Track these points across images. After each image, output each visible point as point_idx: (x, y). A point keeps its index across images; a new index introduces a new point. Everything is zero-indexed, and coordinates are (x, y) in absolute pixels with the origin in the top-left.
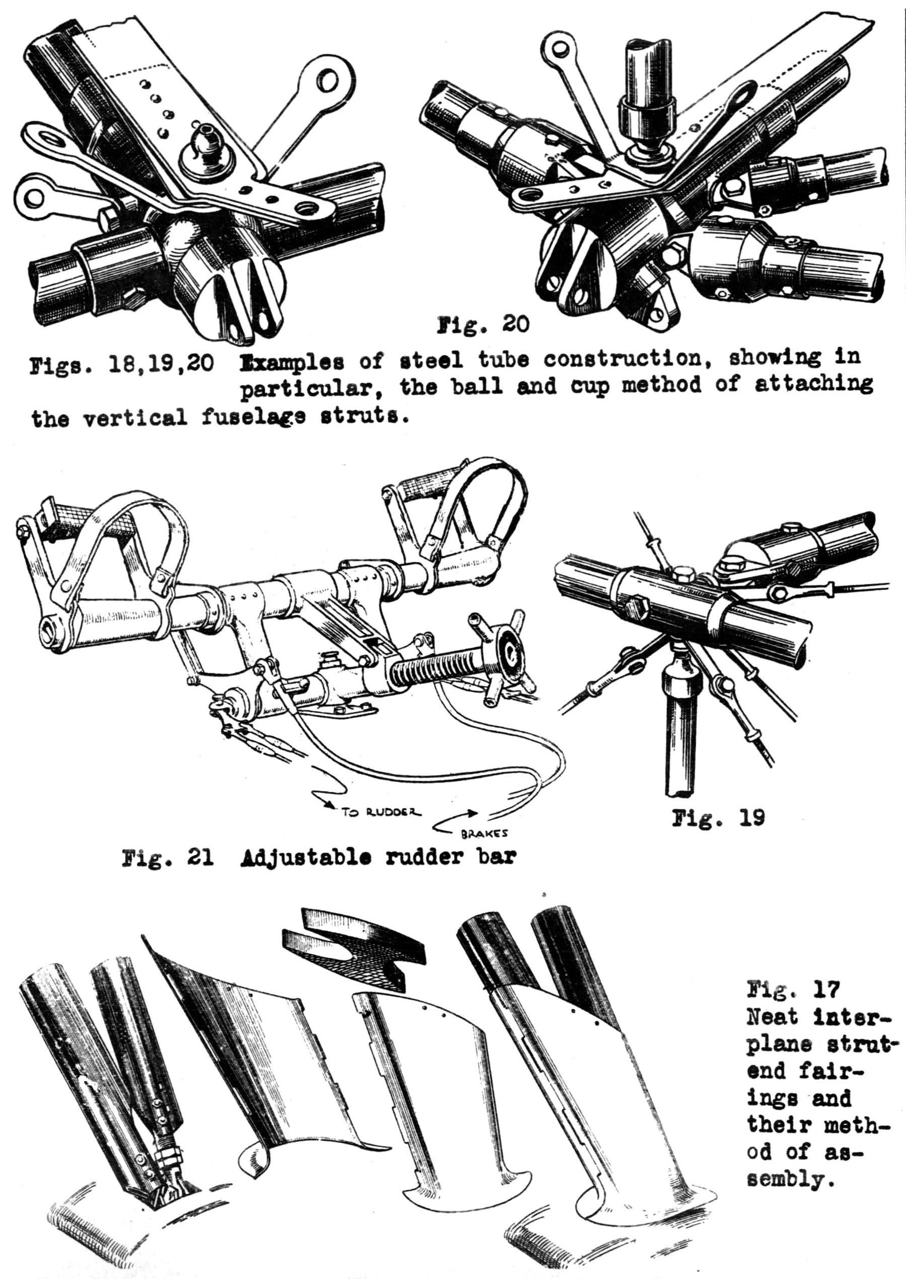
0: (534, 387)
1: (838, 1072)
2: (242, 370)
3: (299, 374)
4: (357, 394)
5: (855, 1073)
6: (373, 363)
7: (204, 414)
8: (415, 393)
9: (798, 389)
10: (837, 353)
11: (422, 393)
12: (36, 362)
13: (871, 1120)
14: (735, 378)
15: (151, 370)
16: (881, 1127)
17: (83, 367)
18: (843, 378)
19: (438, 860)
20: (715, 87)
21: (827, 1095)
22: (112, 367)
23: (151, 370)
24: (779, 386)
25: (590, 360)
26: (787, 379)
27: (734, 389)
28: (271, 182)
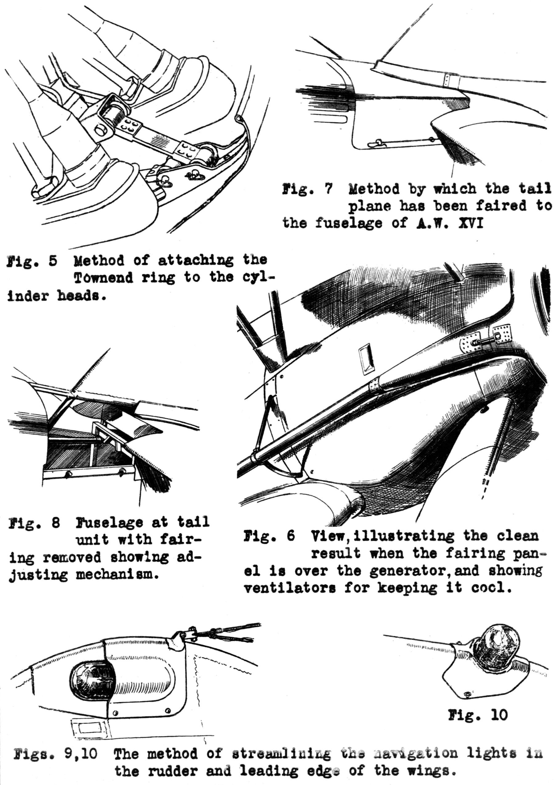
1: (185, 540)
2: (379, 592)
3: (353, 213)
5: (196, 540)
7: (447, 551)
8: (473, 539)
9: (529, 193)
10: (355, 534)
11: (478, 539)
12: (248, 533)
15: (83, 758)
16: (541, 554)
17: (100, 297)
18: (417, 585)
22: (83, 756)
23: (83, 758)
24: (173, 261)
25: (332, 554)
27: (403, 226)
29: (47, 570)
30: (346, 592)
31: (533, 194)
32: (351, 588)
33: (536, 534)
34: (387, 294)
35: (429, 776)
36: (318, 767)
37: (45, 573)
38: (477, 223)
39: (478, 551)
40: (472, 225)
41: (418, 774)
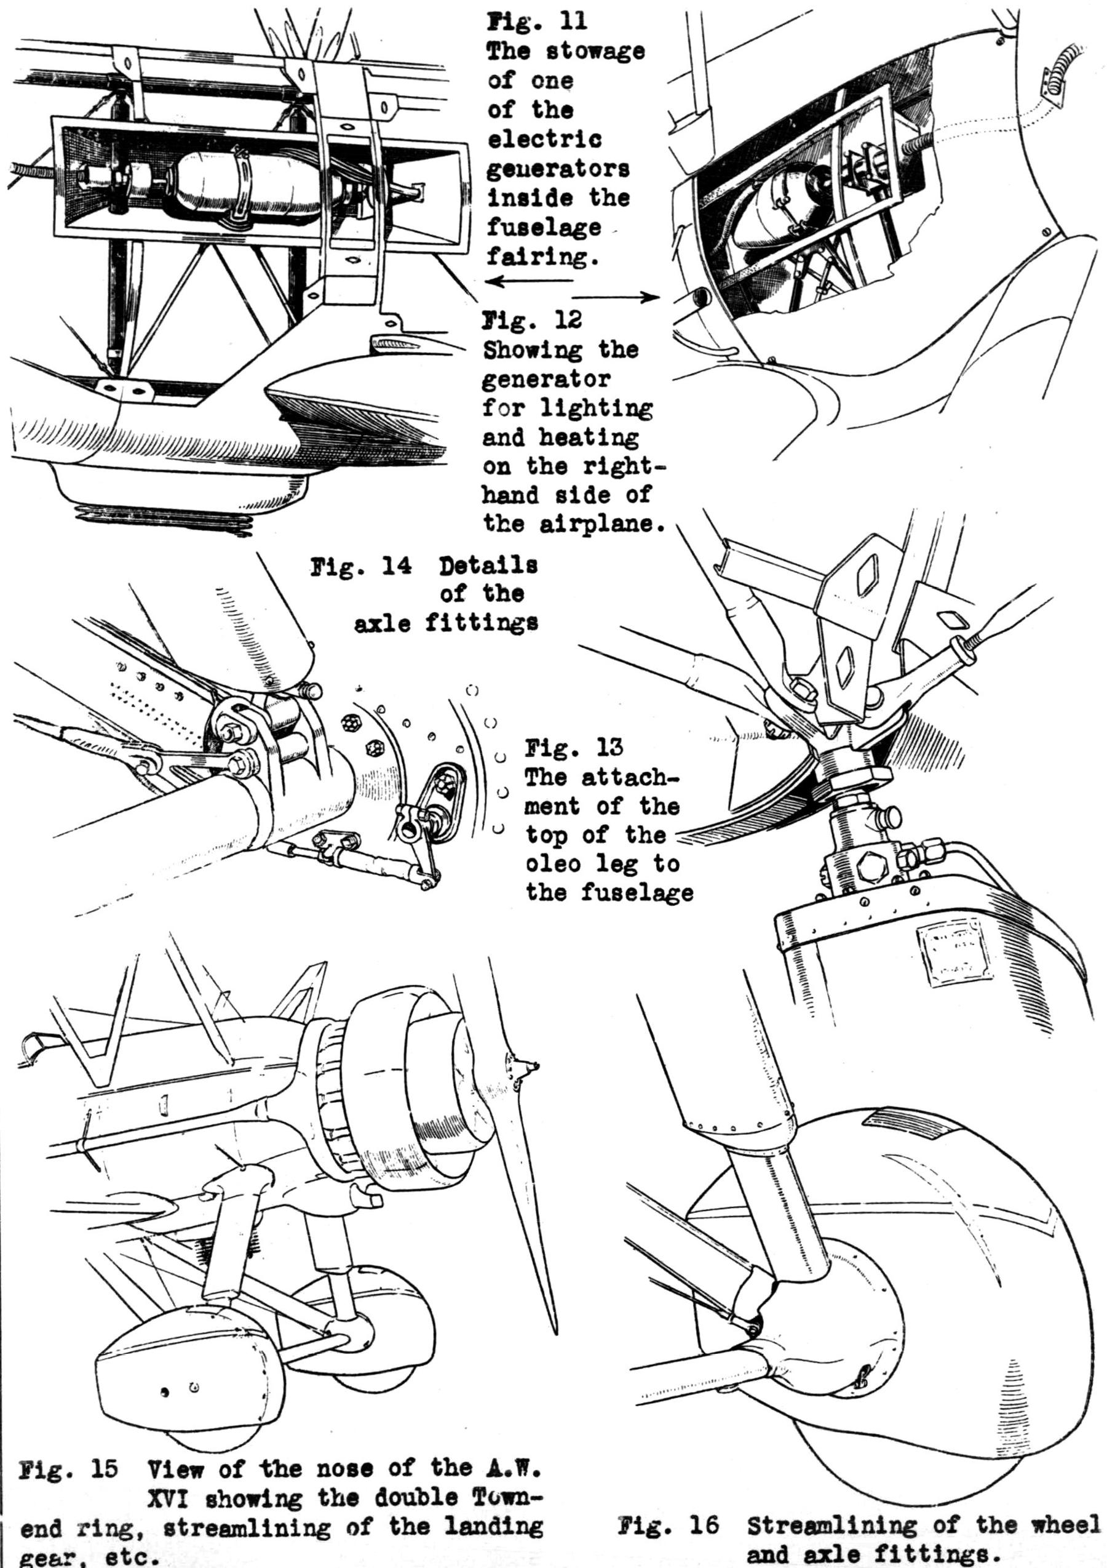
0: (477, 1527)
4: (552, 531)
6: (641, 496)
13: (546, 460)
14: (604, 828)
19: (597, 499)
20: (885, 616)
21: (627, 520)
26: (616, 773)
28: (907, 671)
29: (488, 615)
30: (486, 414)
31: (511, 267)
32: (494, 409)
33: (506, 463)
34: (87, 513)
35: (504, 632)
36: (780, 1549)
37: (485, 619)
38: (177, 1498)
39: (541, 254)
40: (169, 1504)
41: (543, 356)
